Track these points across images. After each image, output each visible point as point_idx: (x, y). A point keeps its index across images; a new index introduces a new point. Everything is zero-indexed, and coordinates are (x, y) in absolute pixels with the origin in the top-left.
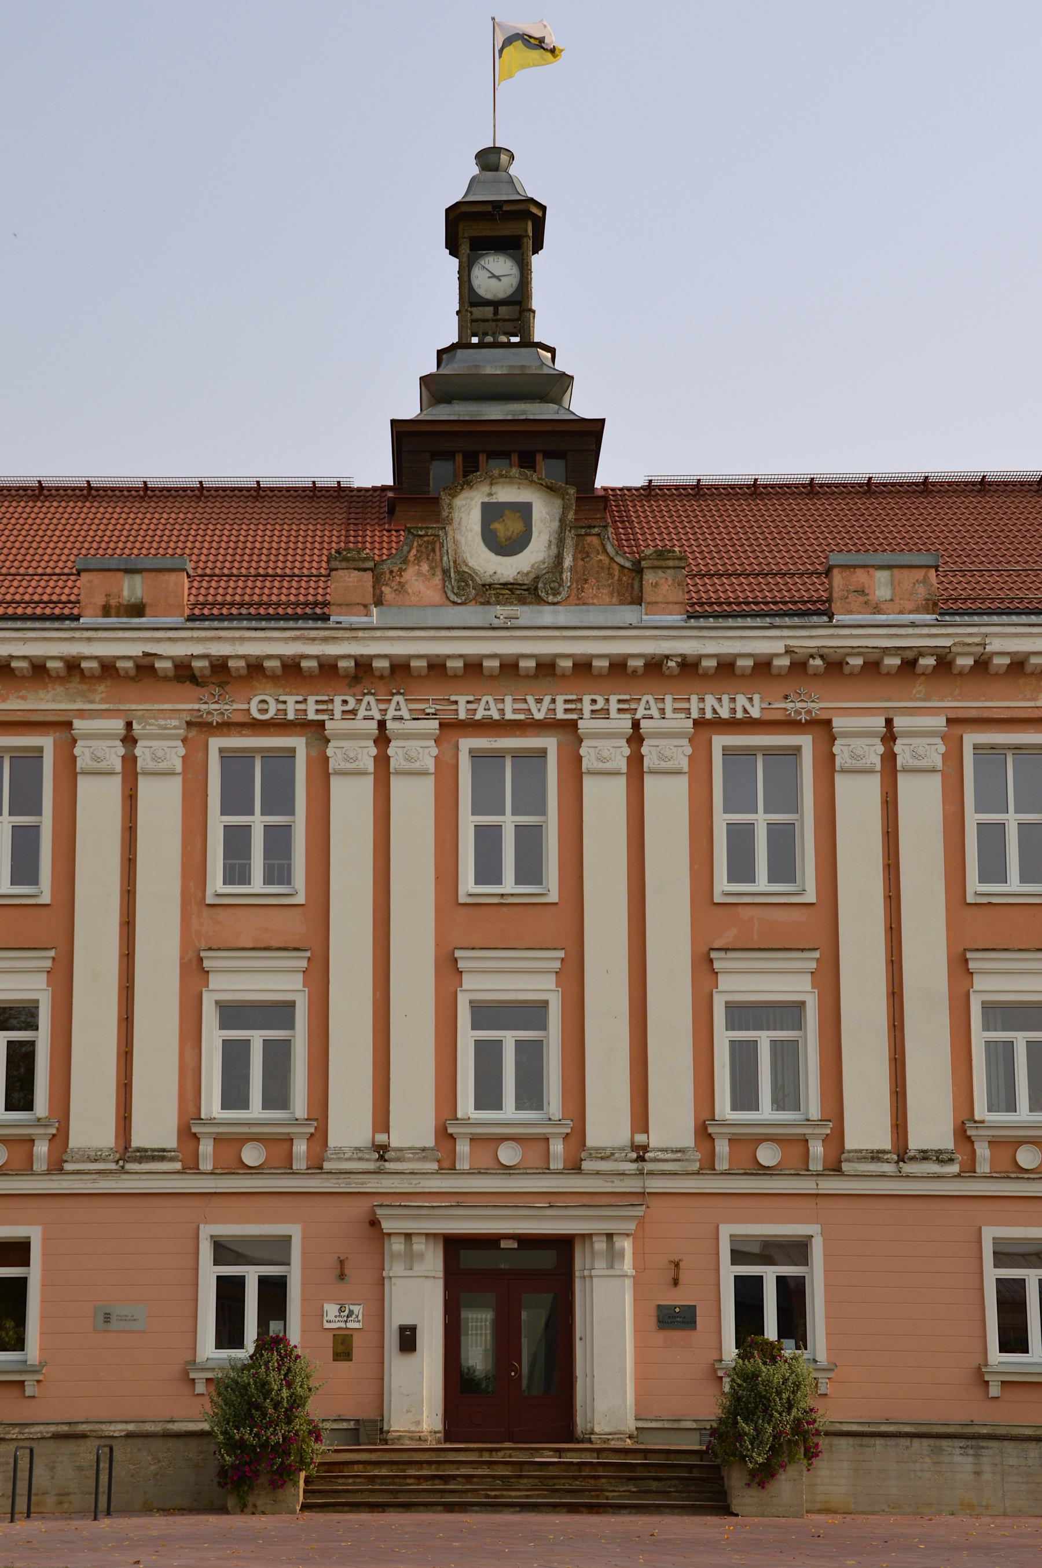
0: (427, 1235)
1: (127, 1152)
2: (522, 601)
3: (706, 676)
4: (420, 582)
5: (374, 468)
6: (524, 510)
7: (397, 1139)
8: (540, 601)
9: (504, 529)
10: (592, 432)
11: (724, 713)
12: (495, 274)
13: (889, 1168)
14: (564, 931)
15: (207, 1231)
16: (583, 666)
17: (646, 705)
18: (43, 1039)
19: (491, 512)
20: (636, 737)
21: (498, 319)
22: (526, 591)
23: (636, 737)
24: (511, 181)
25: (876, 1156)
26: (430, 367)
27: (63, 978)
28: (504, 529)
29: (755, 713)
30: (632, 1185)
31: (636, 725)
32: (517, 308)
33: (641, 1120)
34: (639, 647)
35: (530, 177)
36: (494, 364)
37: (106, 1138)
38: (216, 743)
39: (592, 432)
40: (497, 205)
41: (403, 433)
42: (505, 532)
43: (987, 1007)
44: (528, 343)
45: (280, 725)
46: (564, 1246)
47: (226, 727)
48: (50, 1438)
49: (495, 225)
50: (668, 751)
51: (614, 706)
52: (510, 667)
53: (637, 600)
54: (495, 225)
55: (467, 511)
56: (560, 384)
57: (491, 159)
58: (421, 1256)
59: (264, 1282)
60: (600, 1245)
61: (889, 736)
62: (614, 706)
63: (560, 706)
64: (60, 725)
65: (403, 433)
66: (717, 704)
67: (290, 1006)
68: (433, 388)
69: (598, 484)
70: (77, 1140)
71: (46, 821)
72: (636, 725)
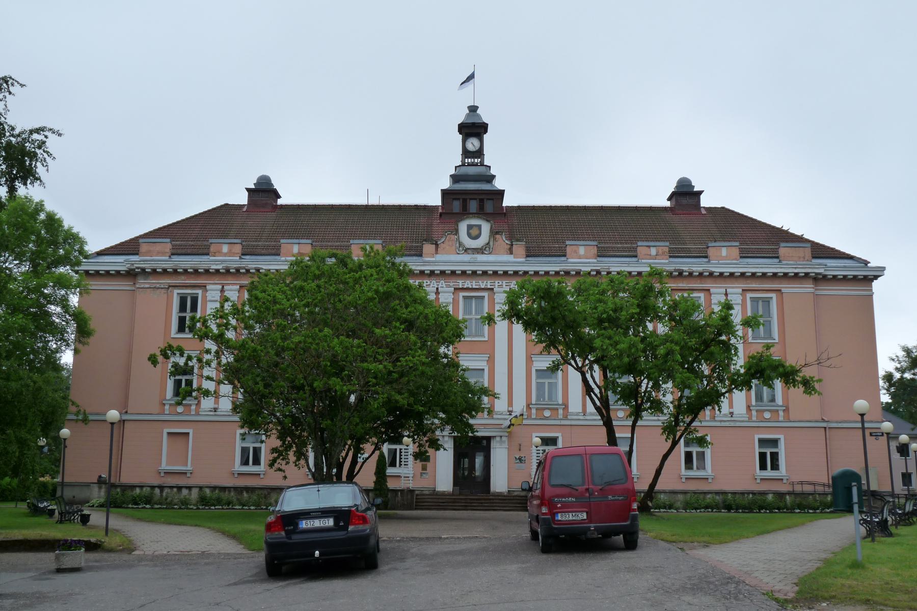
0: (130, 353)
2: (478, 253)
5: (436, 200)
6: (479, 227)
8: (483, 253)
9: (474, 232)
10: (501, 193)
12: (472, 145)
13: (581, 418)
16: (495, 273)
19: (470, 227)
21: (474, 155)
22: (480, 251)
24: (479, 116)
25: (577, 414)
26: (453, 172)
27: (491, 360)
28: (474, 232)
32: (479, 153)
33: (510, 403)
35: (485, 115)
36: (472, 170)
39: (501, 193)
40: (473, 124)
41: (445, 193)
44: (482, 164)
47: (463, 289)
49: (473, 129)
51: (504, 284)
52: (474, 273)
53: (511, 253)
54: (473, 129)
55: (463, 227)
56: (490, 178)
57: (473, 109)
58: (504, 442)
62: (504, 284)
65: (445, 193)
66: (461, 283)
68: (455, 178)
69: (504, 205)
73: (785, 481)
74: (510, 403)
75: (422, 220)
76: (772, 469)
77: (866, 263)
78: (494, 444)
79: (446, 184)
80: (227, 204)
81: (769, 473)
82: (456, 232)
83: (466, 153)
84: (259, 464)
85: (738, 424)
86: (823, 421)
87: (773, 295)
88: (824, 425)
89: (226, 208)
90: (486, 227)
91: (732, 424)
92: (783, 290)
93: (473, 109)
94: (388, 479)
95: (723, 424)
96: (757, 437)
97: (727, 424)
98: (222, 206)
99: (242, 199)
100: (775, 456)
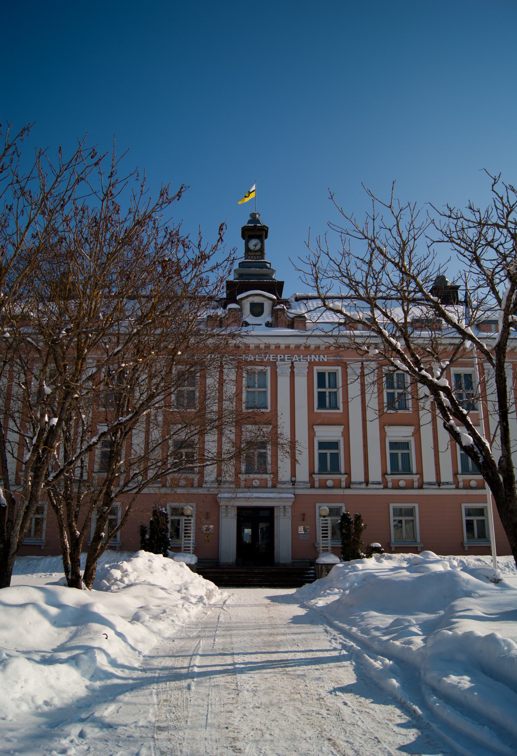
14: (344, 421)
20: (292, 367)
23: (292, 367)
27: (417, 434)
31: (292, 363)
35: (264, 221)
47: (320, 364)
57: (253, 215)
63: (271, 358)
71: (316, 390)
72: (292, 363)
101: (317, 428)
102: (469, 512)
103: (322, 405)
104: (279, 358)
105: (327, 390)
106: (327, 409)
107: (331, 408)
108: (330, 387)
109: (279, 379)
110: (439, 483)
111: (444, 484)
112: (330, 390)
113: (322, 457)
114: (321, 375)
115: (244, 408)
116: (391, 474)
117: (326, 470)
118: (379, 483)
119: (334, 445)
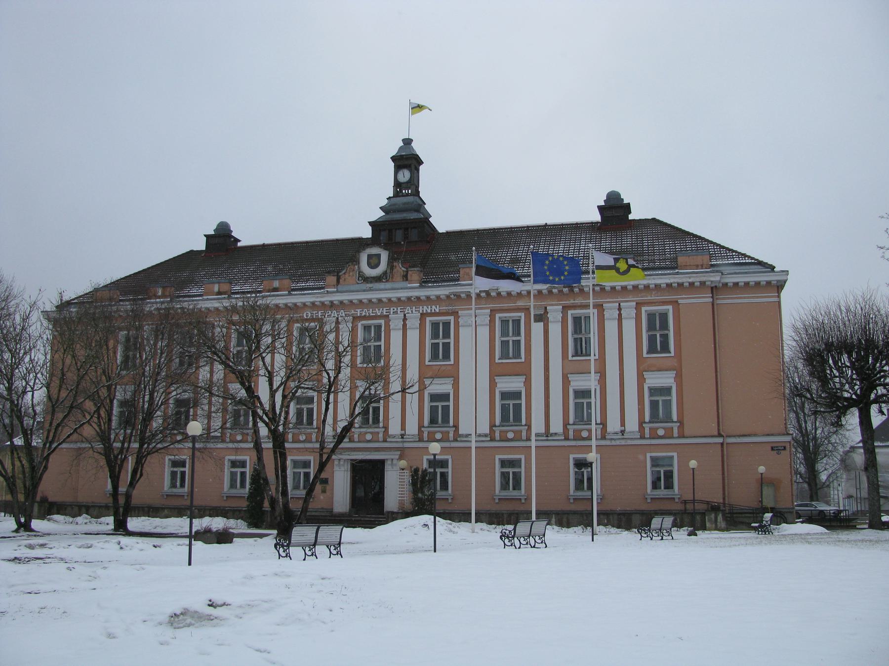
1: (547, 433)
2: (376, 281)
3: (641, 290)
4: (349, 277)
6: (379, 256)
7: (552, 430)
11: (429, 311)
14: (525, 372)
15: (497, 457)
17: (408, 310)
18: (451, 404)
19: (370, 257)
20: (405, 319)
22: (378, 279)
23: (405, 319)
27: (528, 383)
29: (437, 311)
30: (400, 445)
31: (405, 315)
33: (623, 423)
34: (403, 294)
35: (418, 148)
37: (618, 428)
38: (570, 312)
42: (374, 262)
43: (650, 389)
45: (376, 317)
46: (382, 462)
47: (574, 307)
48: (163, 509)
49: (407, 161)
50: (413, 322)
53: (407, 280)
55: (364, 258)
57: (407, 142)
59: (665, 472)
60: (389, 462)
61: (620, 309)
63: (320, 314)
64: (455, 314)
66: (427, 309)
67: (448, 395)
70: (391, 432)
71: (452, 341)
72: (405, 315)
73: (677, 500)
74: (403, 427)
75: (669, 245)
76: (514, 489)
77: (772, 268)
78: (388, 467)
79: (378, 214)
80: (192, 251)
81: (662, 492)
82: (357, 262)
83: (398, 185)
84: (520, 489)
85: (629, 442)
86: (720, 435)
87: (670, 308)
88: (720, 440)
89: (191, 255)
90: (384, 256)
91: (623, 442)
92: (680, 301)
93: (407, 142)
94: (437, 503)
95: (614, 443)
96: (572, 457)
97: (618, 442)
98: (187, 253)
99: (201, 245)
100: (517, 477)
101: (497, 379)
102: (503, 463)
103: (435, 356)
104: (392, 311)
105: (441, 341)
106: (440, 361)
107: (514, 358)
108: (513, 335)
109: (409, 332)
110: (547, 433)
111: (552, 435)
112: (515, 338)
113: (505, 409)
114: (435, 325)
115: (358, 362)
116: (650, 422)
117: (437, 423)
118: (486, 436)
119: (517, 395)
